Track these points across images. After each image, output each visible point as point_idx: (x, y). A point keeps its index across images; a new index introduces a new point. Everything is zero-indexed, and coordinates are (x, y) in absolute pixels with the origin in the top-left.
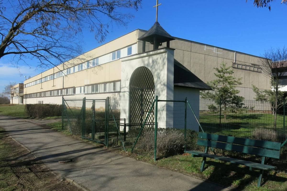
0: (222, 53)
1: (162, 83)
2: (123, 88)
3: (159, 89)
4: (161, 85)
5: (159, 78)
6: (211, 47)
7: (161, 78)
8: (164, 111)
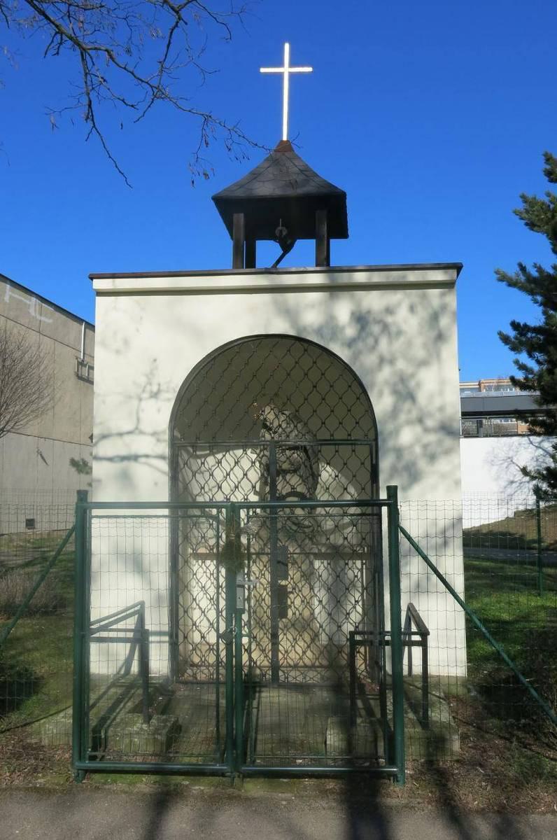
0: (51, 321)
1: (430, 423)
2: (121, 435)
3: (411, 446)
4: (426, 430)
5: (411, 397)
6: (21, 293)
7: (422, 398)
8: (449, 551)
